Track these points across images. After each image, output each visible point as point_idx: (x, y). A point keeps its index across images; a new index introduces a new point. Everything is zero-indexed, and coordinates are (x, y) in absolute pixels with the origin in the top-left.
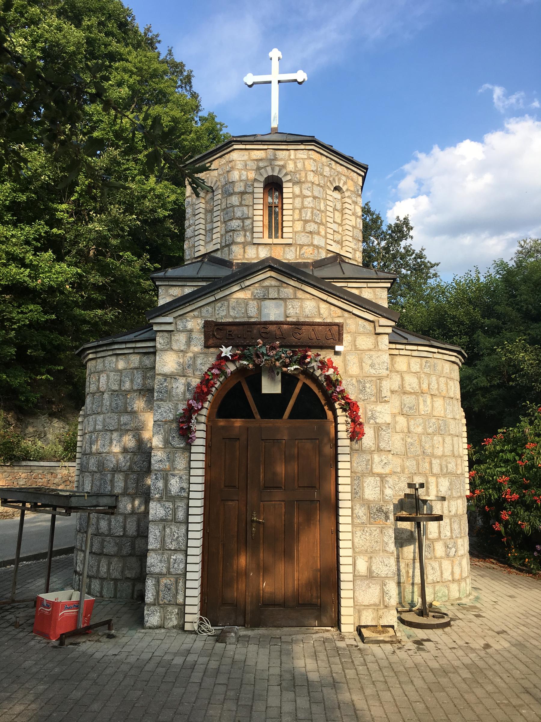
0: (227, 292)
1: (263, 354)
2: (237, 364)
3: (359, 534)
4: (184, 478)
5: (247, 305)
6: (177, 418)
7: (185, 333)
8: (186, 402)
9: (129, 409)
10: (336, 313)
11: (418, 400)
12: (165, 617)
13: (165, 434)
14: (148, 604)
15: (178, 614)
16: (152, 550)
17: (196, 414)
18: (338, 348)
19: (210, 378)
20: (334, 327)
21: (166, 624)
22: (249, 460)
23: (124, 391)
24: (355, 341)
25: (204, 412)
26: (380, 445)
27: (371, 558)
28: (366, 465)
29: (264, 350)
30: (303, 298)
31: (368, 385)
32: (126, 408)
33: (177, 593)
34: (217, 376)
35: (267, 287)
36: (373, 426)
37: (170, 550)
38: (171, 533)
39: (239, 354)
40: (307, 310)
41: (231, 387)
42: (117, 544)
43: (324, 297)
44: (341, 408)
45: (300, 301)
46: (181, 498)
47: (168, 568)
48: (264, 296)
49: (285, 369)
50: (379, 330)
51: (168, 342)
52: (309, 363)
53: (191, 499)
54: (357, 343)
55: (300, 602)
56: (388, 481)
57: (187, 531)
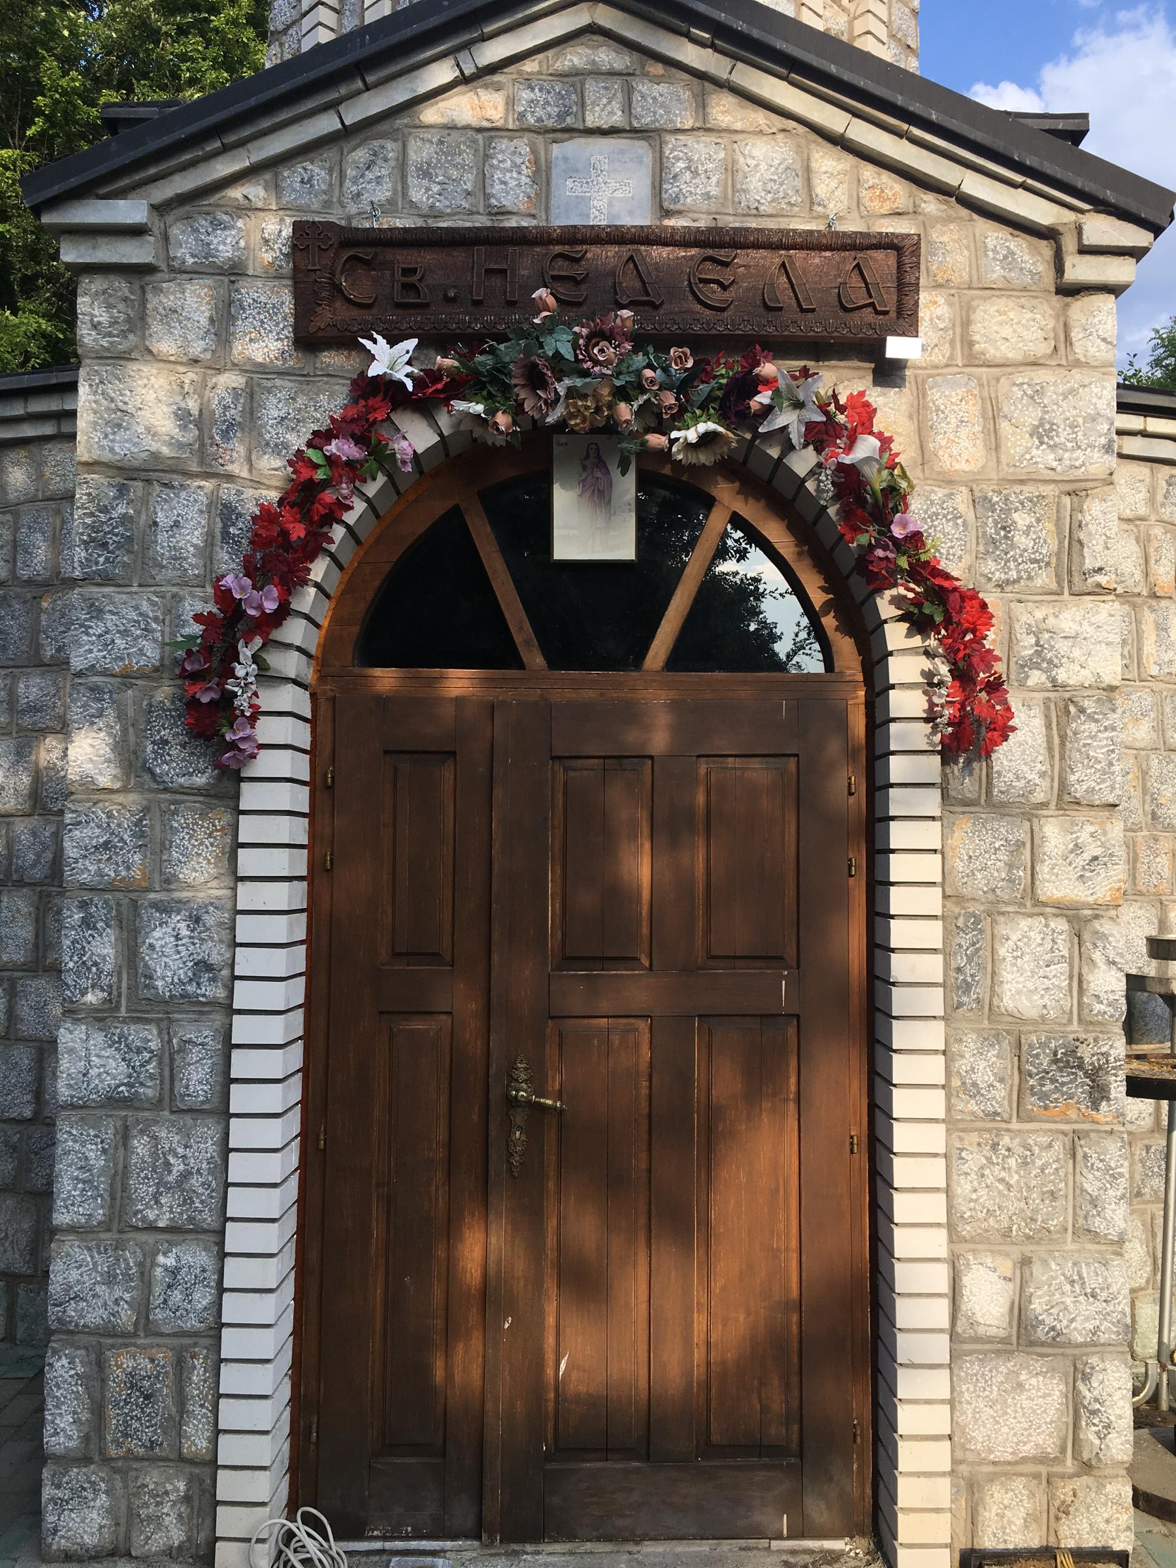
0: (398, 94)
1: (559, 366)
2: (444, 421)
3: (974, 1159)
4: (209, 920)
5: (487, 157)
6: (176, 661)
7: (209, 281)
8: (210, 590)
9: (49, 652)
10: (882, 198)
11: (1138, 622)
12: (132, 1514)
13: (124, 731)
14: (59, 1459)
15: (187, 1499)
16: (72, 1229)
17: (258, 641)
18: (896, 347)
19: (320, 475)
20: (879, 255)
21: (138, 1539)
22: (496, 846)
23: (29, 582)
24: (966, 323)
25: (295, 631)
26: (1073, 778)
27: (1025, 1262)
28: (1010, 866)
29: (561, 344)
30: (738, 126)
31: (1021, 519)
32: (39, 646)
33: (182, 1410)
34: (352, 471)
35: (574, 78)
36: (1040, 696)
37: (152, 1228)
38: (154, 1155)
39: (449, 370)
40: (754, 183)
41: (421, 529)
42: (15, 1148)
43: (833, 119)
44: (901, 619)
45: (725, 140)
46: (200, 1008)
47: (143, 1308)
48: (561, 117)
49: (656, 440)
50: (1080, 270)
51: (129, 320)
52: (767, 410)
53: (240, 1012)
54: (978, 332)
55: (715, 1438)
56: (1104, 937)
57: (226, 1150)
